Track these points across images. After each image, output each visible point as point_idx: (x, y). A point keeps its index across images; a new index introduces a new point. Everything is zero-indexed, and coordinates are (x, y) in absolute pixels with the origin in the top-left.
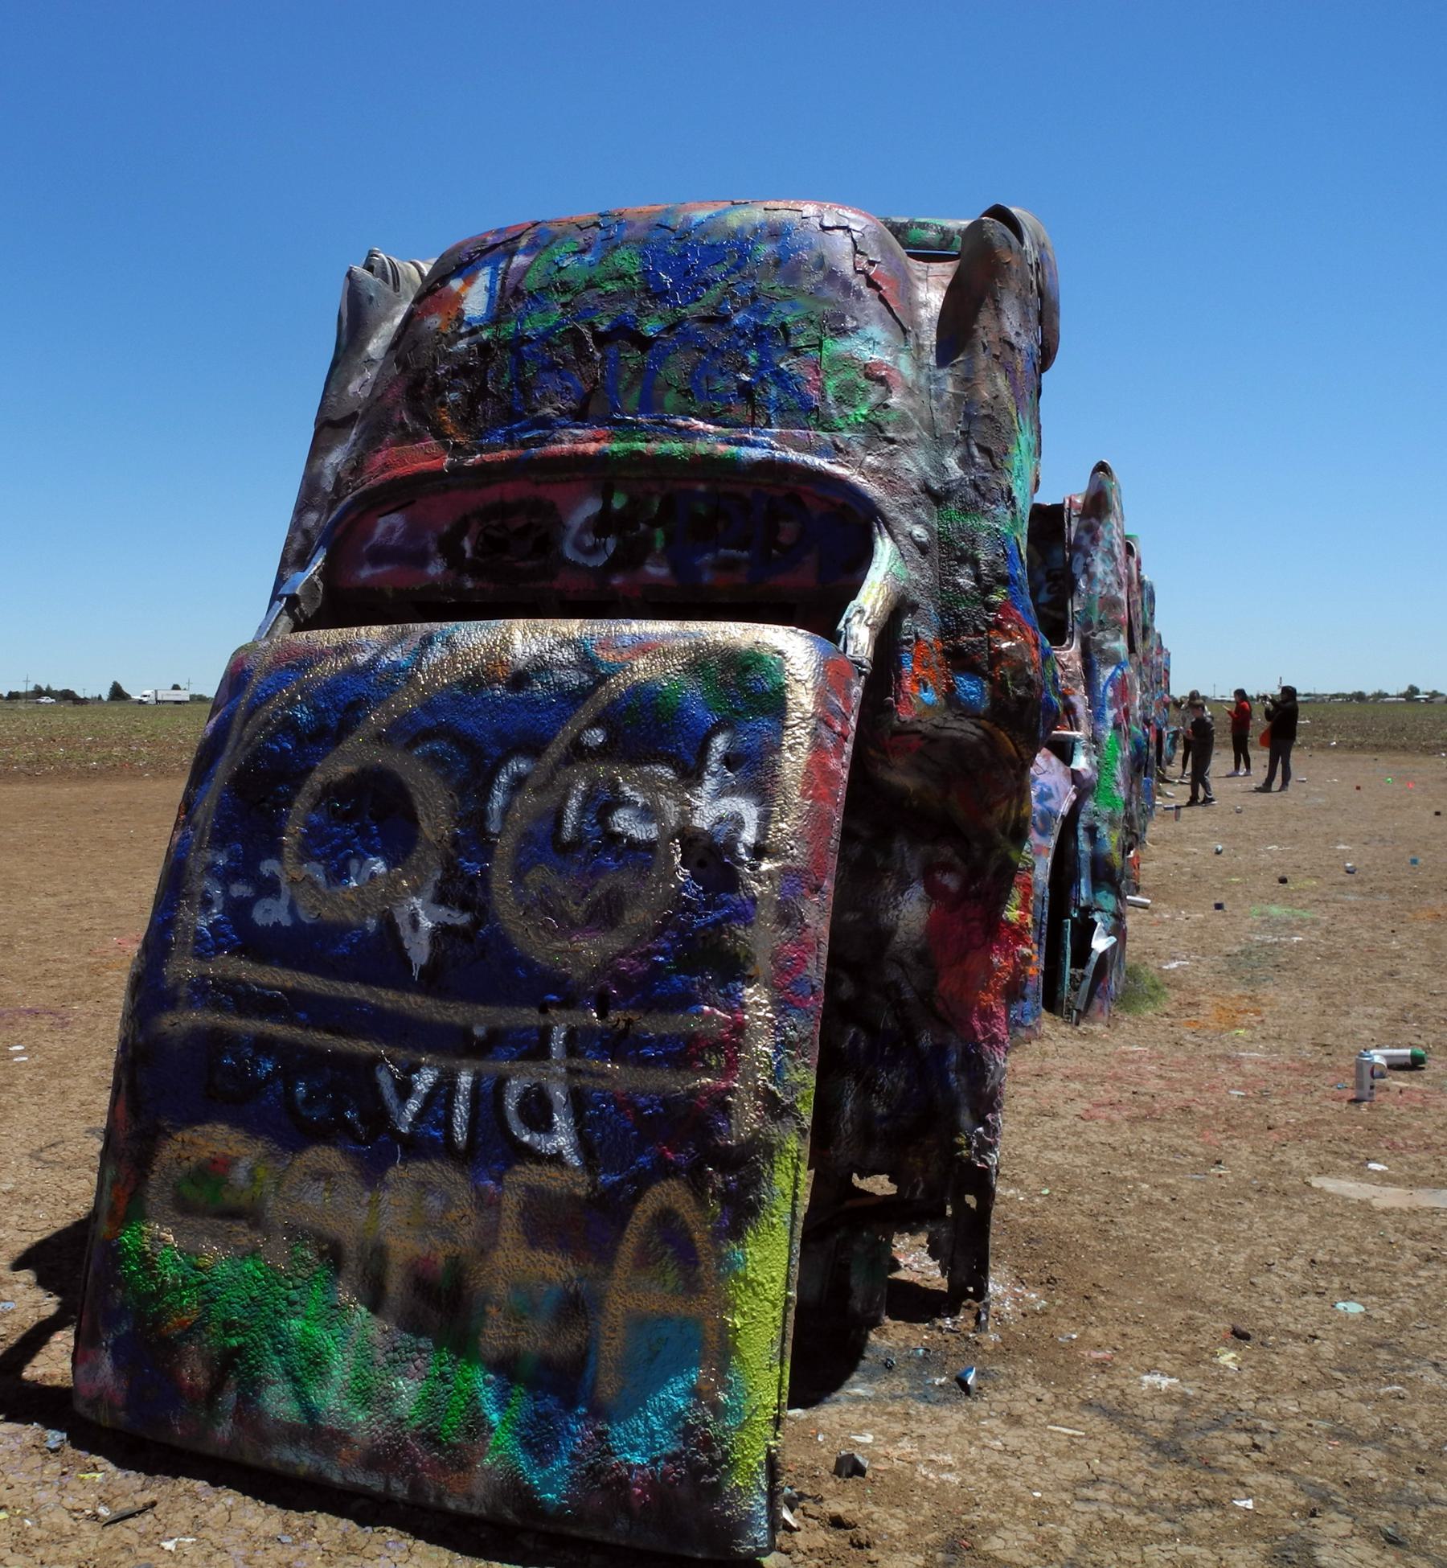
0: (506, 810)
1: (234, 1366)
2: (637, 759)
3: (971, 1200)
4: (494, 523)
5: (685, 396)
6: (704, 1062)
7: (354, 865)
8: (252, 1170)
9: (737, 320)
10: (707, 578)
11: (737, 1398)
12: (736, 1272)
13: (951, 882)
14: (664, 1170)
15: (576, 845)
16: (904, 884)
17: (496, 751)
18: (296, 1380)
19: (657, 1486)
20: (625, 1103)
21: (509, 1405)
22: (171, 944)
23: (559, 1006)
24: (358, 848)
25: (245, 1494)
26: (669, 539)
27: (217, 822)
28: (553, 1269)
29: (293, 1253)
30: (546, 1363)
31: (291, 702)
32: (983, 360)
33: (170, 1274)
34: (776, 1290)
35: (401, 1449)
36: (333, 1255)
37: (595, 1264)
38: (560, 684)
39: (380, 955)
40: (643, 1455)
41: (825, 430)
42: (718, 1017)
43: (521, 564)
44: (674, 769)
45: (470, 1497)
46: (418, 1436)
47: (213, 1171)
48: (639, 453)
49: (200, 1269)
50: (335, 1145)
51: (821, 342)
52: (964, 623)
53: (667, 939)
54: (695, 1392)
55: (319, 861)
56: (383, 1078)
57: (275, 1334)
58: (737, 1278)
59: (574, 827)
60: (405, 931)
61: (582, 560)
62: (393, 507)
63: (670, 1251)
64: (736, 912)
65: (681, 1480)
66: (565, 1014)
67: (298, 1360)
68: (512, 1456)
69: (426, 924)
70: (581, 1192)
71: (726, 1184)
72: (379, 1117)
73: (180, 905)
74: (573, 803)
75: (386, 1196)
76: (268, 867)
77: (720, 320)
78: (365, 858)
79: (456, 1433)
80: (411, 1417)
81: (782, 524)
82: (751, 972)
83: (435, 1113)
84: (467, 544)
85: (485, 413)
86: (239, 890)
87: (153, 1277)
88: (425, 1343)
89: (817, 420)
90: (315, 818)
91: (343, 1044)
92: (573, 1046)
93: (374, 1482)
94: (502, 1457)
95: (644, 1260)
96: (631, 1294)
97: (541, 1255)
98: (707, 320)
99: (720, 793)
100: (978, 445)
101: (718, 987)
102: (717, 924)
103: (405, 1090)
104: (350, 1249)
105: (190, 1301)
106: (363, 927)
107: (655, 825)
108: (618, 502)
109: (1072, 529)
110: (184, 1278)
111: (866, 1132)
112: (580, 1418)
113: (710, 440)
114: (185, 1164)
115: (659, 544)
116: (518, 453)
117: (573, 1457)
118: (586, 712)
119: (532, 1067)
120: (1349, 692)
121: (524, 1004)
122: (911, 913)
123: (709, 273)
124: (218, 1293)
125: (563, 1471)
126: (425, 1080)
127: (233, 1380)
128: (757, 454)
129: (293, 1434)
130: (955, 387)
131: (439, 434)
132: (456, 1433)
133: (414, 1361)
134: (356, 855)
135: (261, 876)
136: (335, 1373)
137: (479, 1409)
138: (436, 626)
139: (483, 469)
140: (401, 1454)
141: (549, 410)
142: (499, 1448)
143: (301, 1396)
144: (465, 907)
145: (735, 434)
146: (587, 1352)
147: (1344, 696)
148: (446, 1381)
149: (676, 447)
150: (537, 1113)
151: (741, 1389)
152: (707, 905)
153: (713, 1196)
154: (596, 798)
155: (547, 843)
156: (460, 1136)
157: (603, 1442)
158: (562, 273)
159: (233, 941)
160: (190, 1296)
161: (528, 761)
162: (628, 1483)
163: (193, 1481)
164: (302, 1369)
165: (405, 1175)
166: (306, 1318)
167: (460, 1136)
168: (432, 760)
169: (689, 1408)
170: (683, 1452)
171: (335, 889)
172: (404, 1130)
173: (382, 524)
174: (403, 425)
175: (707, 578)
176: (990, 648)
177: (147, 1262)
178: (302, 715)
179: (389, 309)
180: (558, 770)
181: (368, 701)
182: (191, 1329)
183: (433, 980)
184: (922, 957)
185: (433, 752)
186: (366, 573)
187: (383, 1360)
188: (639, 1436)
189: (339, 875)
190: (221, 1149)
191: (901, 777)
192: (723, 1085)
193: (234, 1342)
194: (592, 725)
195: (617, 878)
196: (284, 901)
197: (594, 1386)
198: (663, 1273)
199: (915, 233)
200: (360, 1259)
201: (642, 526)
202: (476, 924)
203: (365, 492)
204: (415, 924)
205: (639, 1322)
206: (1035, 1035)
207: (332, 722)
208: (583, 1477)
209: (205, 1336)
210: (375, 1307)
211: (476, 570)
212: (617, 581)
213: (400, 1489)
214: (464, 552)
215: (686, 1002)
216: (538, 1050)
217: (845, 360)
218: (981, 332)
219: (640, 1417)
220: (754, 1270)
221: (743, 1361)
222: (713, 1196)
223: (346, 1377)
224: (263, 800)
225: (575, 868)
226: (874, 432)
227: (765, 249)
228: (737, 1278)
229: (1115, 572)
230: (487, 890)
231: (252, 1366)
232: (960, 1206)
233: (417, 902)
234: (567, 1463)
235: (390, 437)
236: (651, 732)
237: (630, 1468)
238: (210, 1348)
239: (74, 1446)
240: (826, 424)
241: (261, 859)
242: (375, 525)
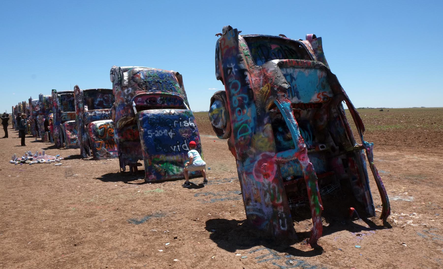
82: (28, 140)
86: (153, 133)
93: (181, 177)
103: (174, 148)
113: (170, 93)
126: (175, 147)
129: (173, 176)
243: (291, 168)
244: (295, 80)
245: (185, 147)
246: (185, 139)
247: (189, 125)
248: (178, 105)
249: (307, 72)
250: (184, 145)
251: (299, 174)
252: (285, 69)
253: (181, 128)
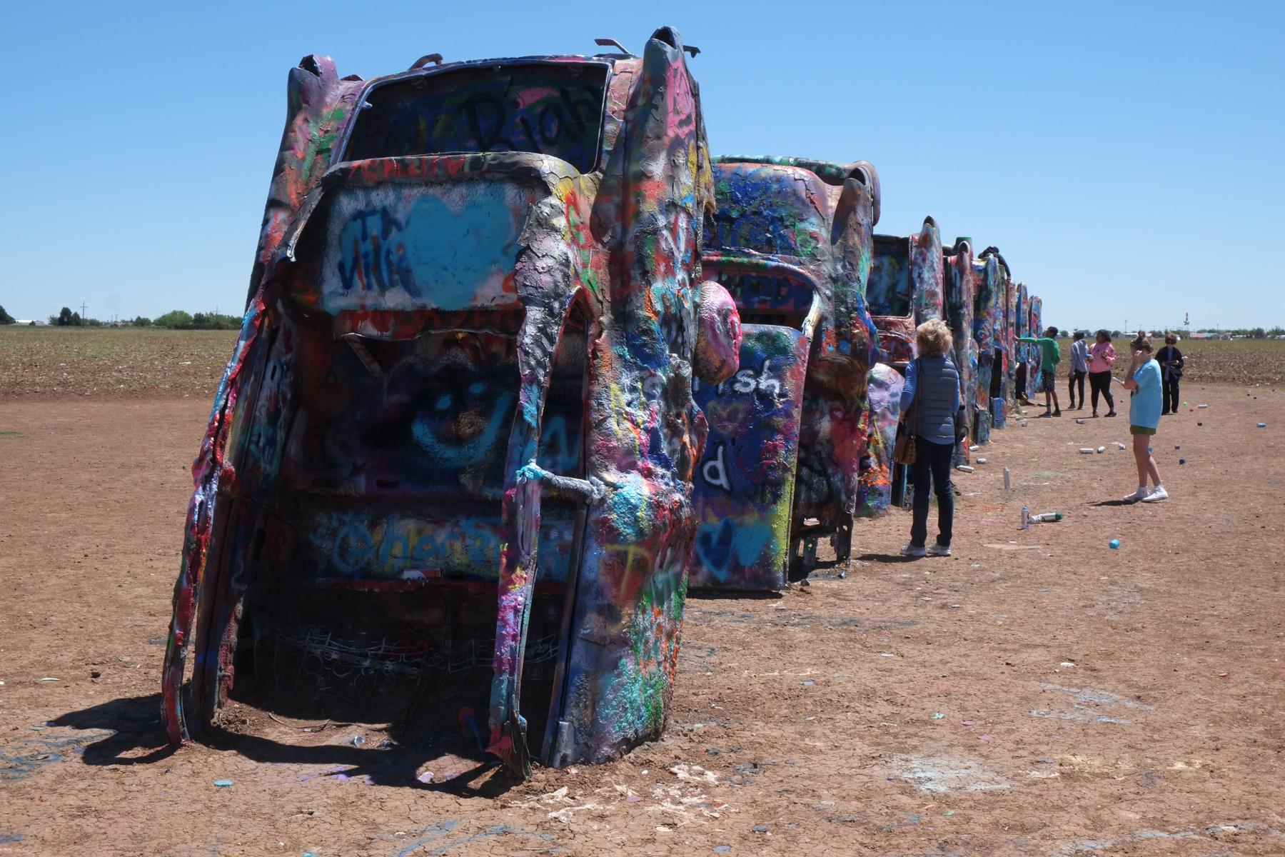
3: (845, 527)
9: (765, 213)
10: (756, 306)
13: (839, 415)
15: (723, 394)
16: (822, 415)
32: (850, 231)
34: (786, 518)
77: (757, 213)
98: (754, 213)
109: (913, 253)
111: (809, 504)
113: (758, 257)
120: (1249, 329)
122: (825, 426)
123: (755, 195)
128: (774, 264)
147: (1244, 332)
149: (746, 260)
175: (756, 306)
184: (829, 441)
191: (822, 376)
199: (828, 169)
206: (886, 512)
226: (813, 257)
227: (775, 187)
229: (934, 277)
232: (841, 529)
243: (458, 545)
244: (400, 228)
245: (714, 473)
246: (722, 442)
247: (757, 389)
249: (455, 197)
250: (711, 463)
251: (485, 573)
252: (360, 195)
253: (719, 396)
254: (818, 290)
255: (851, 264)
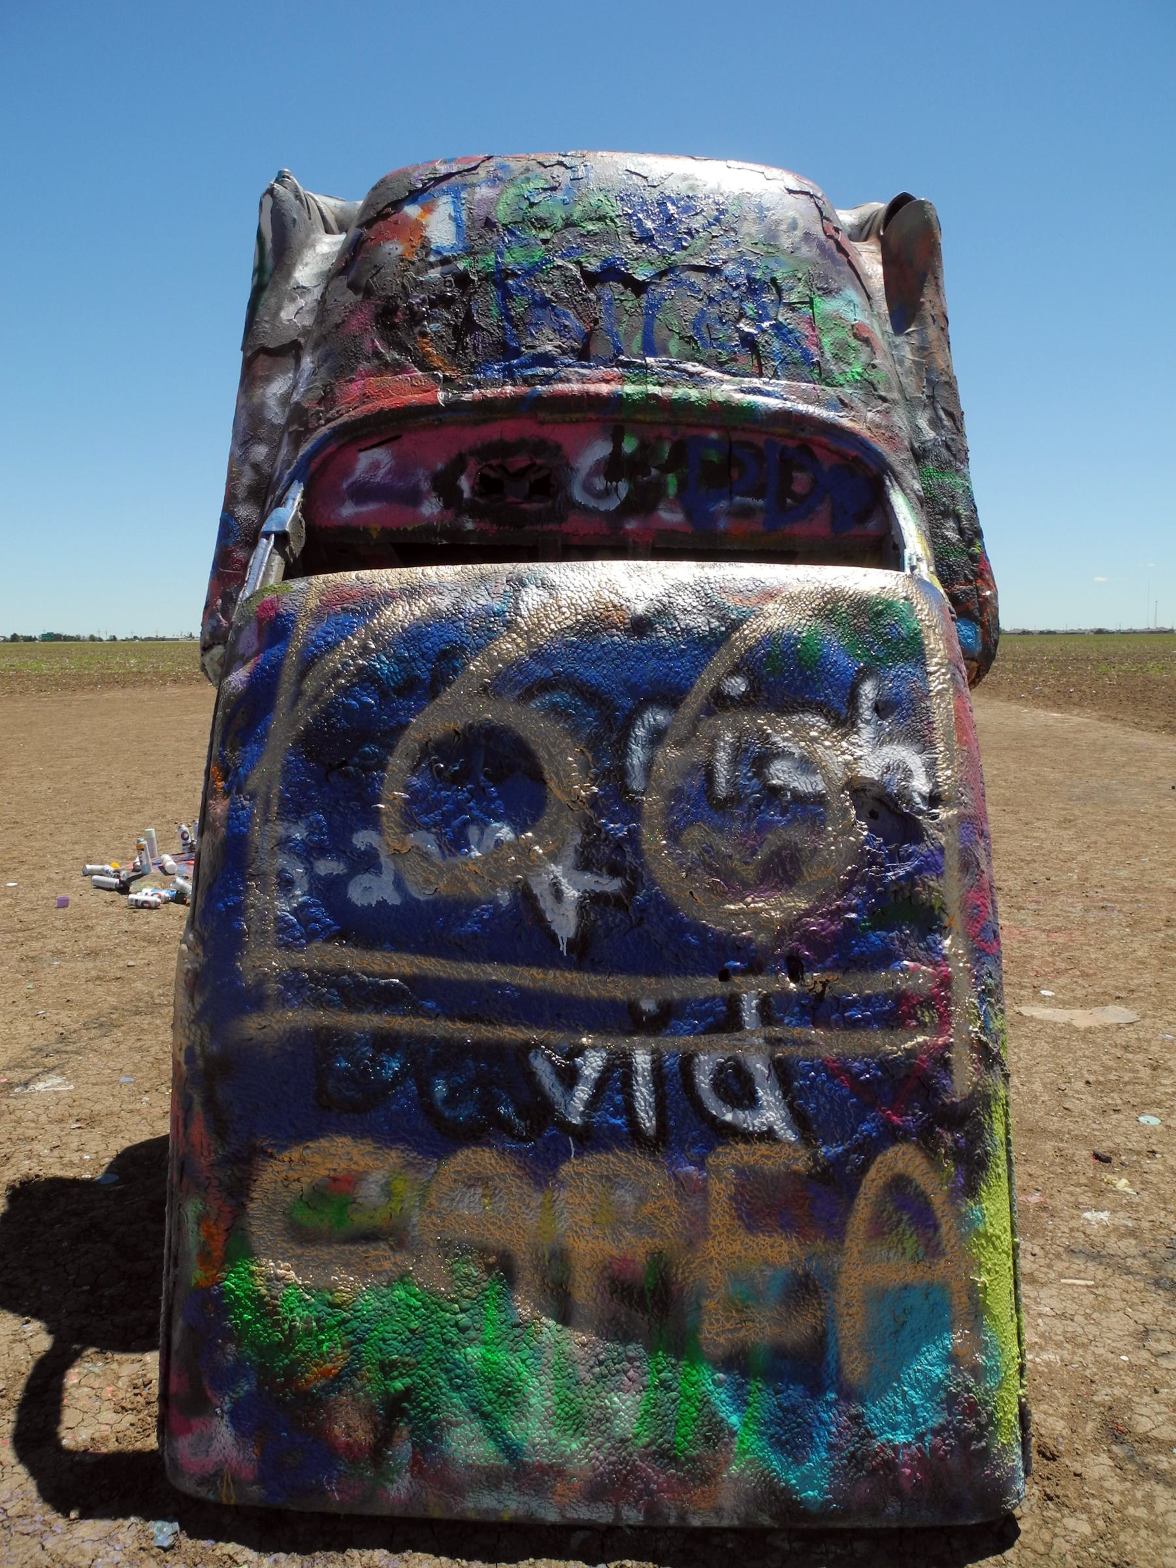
0: (648, 767)
1: (403, 1412)
2: (785, 708)
4: (494, 462)
5: (688, 343)
6: (917, 1020)
7: (473, 832)
8: (388, 1184)
10: (722, 524)
11: (993, 1356)
12: (977, 1230)
14: (891, 1135)
15: (734, 800)
17: (628, 702)
18: (485, 1416)
19: (927, 1462)
20: (837, 1070)
21: (748, 1404)
22: (243, 934)
23: (744, 972)
24: (476, 813)
25: (437, 1555)
26: (682, 486)
27: (287, 790)
28: (778, 1251)
29: (453, 1272)
30: (779, 1352)
31: (364, 650)
33: (299, 1317)
35: (629, 1473)
36: (504, 1268)
37: (825, 1242)
38: (688, 631)
39: (519, 928)
40: (907, 1432)
41: (828, 384)
42: (923, 972)
43: (526, 506)
44: (826, 717)
45: (718, 1511)
46: (648, 1455)
47: (335, 1192)
48: (655, 396)
49: (338, 1306)
50: (490, 1146)
51: (812, 299)
52: (956, 573)
53: (857, 895)
54: (951, 1358)
55: (428, 830)
56: (541, 1067)
57: (450, 1368)
58: (979, 1235)
59: (728, 781)
60: (546, 903)
61: (592, 503)
62: (376, 441)
63: (905, 1217)
64: (928, 863)
65: (951, 1452)
66: (753, 980)
67: (484, 1394)
68: (762, 1459)
69: (571, 894)
70: (800, 1166)
71: (956, 1141)
72: (541, 1110)
73: (247, 887)
74: (722, 756)
75: (564, 1194)
76: (362, 839)
78: (487, 824)
79: (693, 1445)
80: (636, 1436)
81: (795, 474)
83: (611, 1098)
84: (464, 484)
85: (475, 347)
86: (327, 867)
87: (276, 1324)
88: (633, 1349)
89: (820, 374)
90: (415, 781)
91: (487, 1033)
92: (768, 1012)
93: (602, 1514)
94: (750, 1462)
95: (879, 1230)
96: (866, 1266)
97: (763, 1240)
99: (880, 741)
100: (943, 409)
101: (918, 941)
102: (909, 875)
103: (569, 1077)
104: (523, 1259)
105: (333, 1347)
106: (493, 901)
107: (819, 777)
108: (629, 445)
110: (318, 1320)
112: (830, 1405)
114: (295, 1186)
115: (672, 490)
116: (524, 389)
117: (831, 1447)
118: (720, 662)
119: (724, 1039)
121: (704, 973)
124: (367, 1331)
125: (822, 1464)
126: (592, 1064)
127: (404, 1428)
128: (773, 403)
129: (492, 1479)
130: (913, 354)
131: (424, 367)
132: (693, 1445)
133: (625, 1372)
134: (473, 820)
135: (354, 849)
136: (533, 1401)
137: (714, 1414)
138: (522, 567)
139: (486, 406)
140: (630, 1478)
141: (550, 348)
142: (746, 1452)
143: (495, 1433)
144: (614, 871)
145: (748, 382)
146: (825, 1333)
148: (669, 1389)
150: (737, 1087)
151: (996, 1347)
152: (894, 856)
153: (946, 1156)
154: (746, 750)
155: (700, 799)
156: (647, 1121)
157: (859, 1425)
158: (535, 209)
159: (330, 926)
160: (330, 1340)
161: (664, 712)
162: (896, 1465)
163: (368, 1553)
164: (490, 1402)
165: (581, 1169)
166: (485, 1343)
167: (647, 1121)
168: (556, 712)
169: (948, 1376)
170: (949, 1423)
171: (451, 860)
172: (576, 1120)
173: (364, 460)
174: (377, 354)
175: (722, 524)
176: (979, 596)
177: (265, 1308)
178: (383, 665)
179: (308, 236)
180: (700, 720)
181: (463, 650)
182: (338, 1377)
183: (584, 952)
185: (555, 705)
186: (348, 511)
187: (588, 1377)
188: (899, 1413)
189: (457, 843)
190: (340, 1165)
192: (940, 1041)
193: (398, 1385)
194: (735, 671)
195: (787, 833)
196: (387, 877)
197: (839, 1370)
198: (900, 1241)
200: (536, 1268)
201: (654, 472)
202: (631, 890)
203: (345, 424)
204: (558, 894)
205: (878, 1295)
207: (423, 671)
208: (845, 1467)
209: (358, 1383)
210: (565, 1318)
211: (473, 510)
212: (631, 525)
213: (633, 1516)
214: (461, 492)
215: (886, 958)
216: (726, 1019)
217: (834, 318)
218: (928, 305)
219: (896, 1394)
220: (992, 1225)
221: (994, 1318)
222: (946, 1156)
223: (548, 1403)
224: (345, 764)
225: (737, 825)
228: (979, 1235)
230: (638, 853)
231: (425, 1410)
233: (557, 870)
234: (824, 1455)
235: (364, 366)
236: (790, 678)
237: (895, 1449)
238: (367, 1395)
239: (191, 1536)
240: (826, 379)
241: (353, 830)
242: (356, 460)
248: (819, 524)
254: (897, 477)
255: (950, 415)
